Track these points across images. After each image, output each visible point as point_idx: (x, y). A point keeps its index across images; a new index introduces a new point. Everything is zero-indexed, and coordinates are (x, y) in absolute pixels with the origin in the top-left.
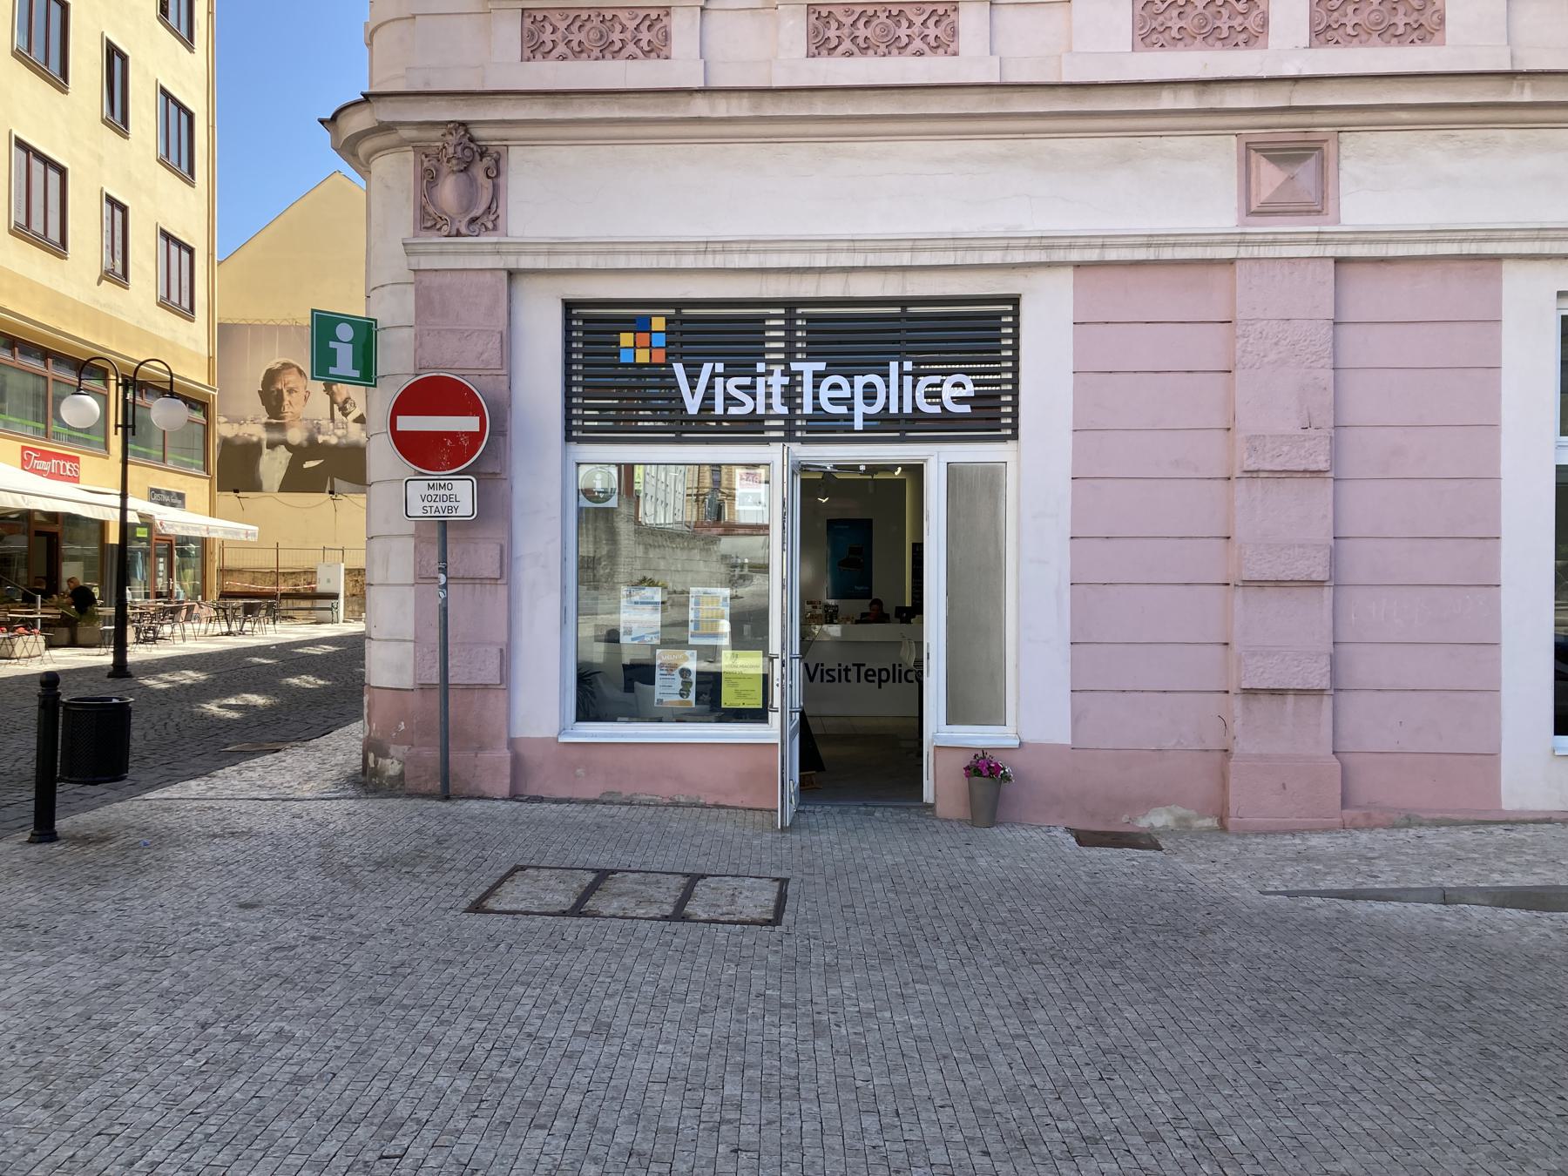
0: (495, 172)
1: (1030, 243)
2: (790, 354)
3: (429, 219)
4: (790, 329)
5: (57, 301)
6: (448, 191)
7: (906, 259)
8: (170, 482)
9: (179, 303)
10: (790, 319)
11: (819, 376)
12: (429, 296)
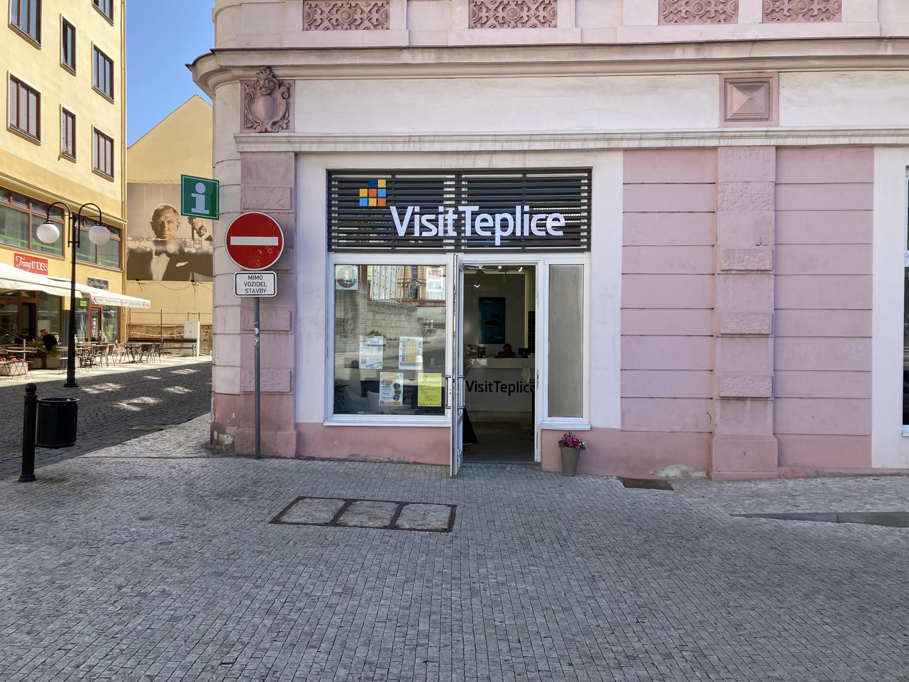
0: (288, 95)
1: (598, 137)
2: (458, 202)
3: (249, 123)
4: (458, 187)
5: (35, 170)
6: (260, 106)
7: (526, 146)
10: (458, 181)
11: (475, 214)
12: (250, 167)
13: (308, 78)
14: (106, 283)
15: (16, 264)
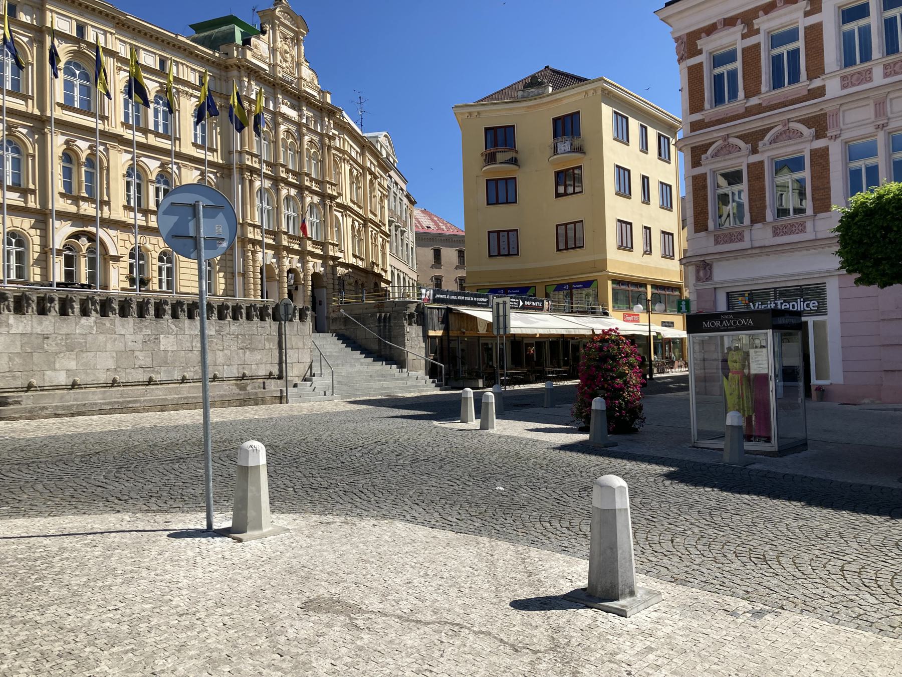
0: (711, 269)
1: (825, 272)
2: (776, 299)
3: (698, 279)
4: (775, 294)
5: (632, 266)
6: (701, 273)
7: (797, 278)
8: (668, 318)
9: (668, 255)
10: (775, 291)
13: (721, 260)
14: (673, 323)
15: (625, 320)
